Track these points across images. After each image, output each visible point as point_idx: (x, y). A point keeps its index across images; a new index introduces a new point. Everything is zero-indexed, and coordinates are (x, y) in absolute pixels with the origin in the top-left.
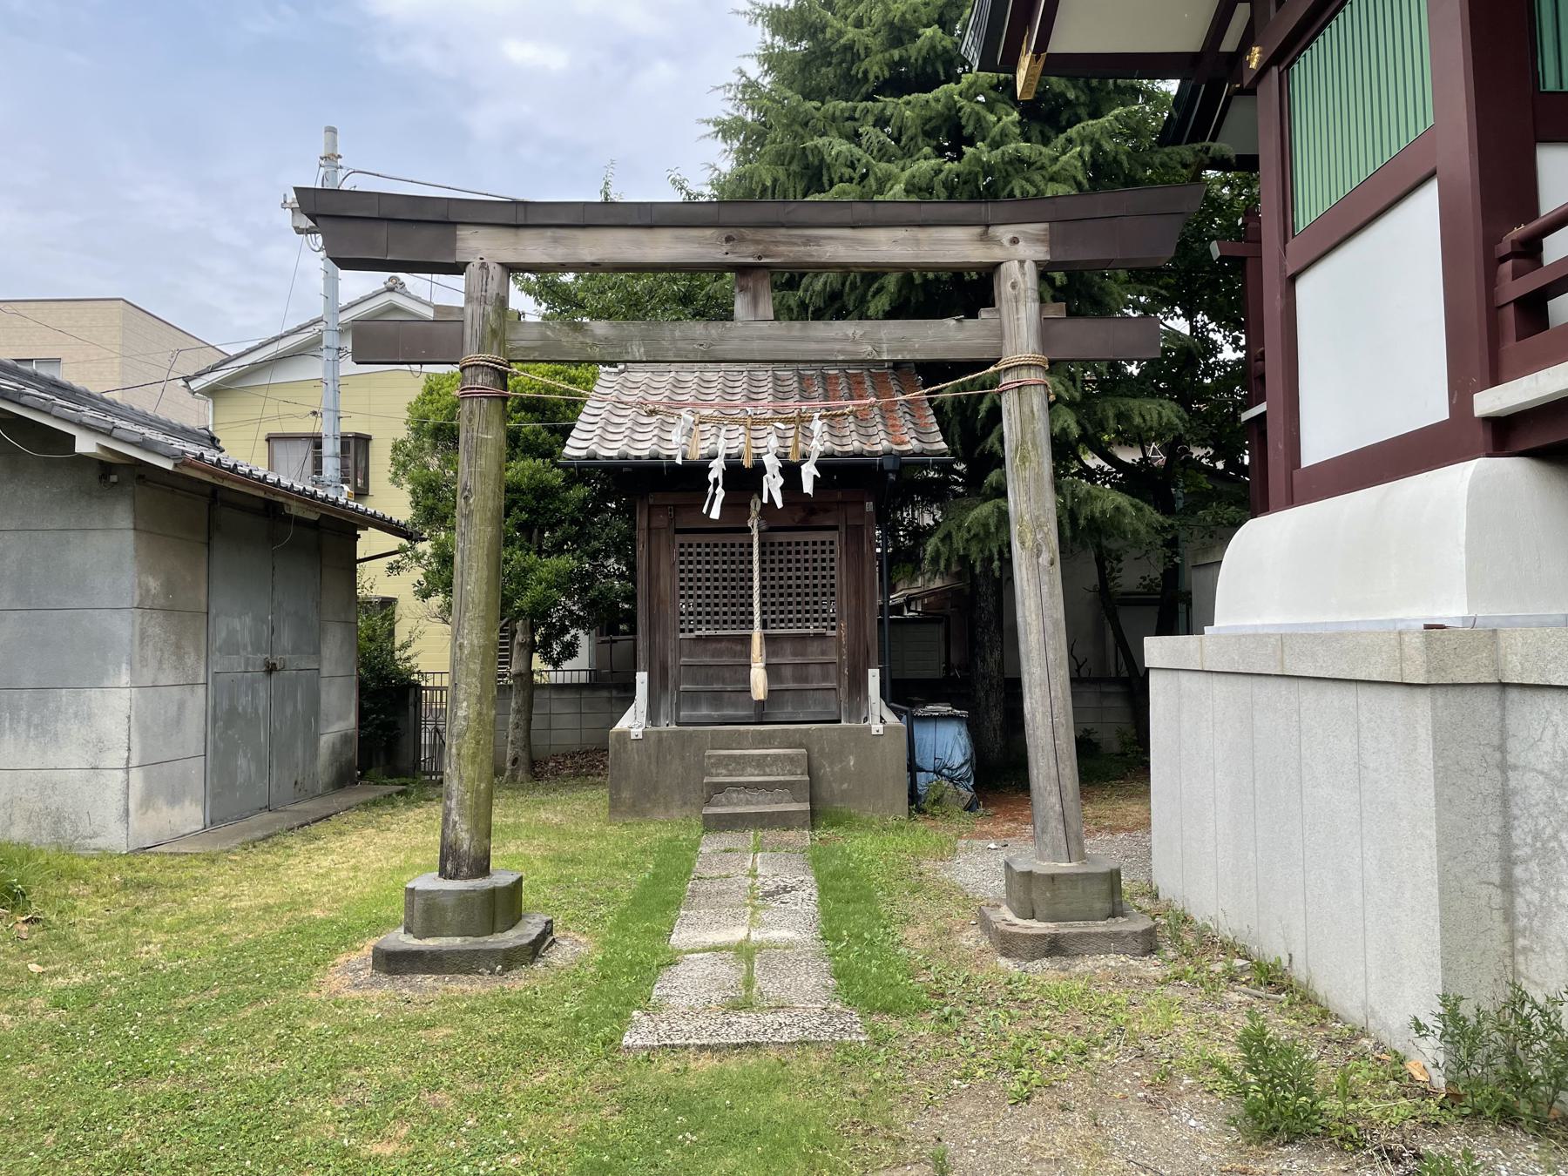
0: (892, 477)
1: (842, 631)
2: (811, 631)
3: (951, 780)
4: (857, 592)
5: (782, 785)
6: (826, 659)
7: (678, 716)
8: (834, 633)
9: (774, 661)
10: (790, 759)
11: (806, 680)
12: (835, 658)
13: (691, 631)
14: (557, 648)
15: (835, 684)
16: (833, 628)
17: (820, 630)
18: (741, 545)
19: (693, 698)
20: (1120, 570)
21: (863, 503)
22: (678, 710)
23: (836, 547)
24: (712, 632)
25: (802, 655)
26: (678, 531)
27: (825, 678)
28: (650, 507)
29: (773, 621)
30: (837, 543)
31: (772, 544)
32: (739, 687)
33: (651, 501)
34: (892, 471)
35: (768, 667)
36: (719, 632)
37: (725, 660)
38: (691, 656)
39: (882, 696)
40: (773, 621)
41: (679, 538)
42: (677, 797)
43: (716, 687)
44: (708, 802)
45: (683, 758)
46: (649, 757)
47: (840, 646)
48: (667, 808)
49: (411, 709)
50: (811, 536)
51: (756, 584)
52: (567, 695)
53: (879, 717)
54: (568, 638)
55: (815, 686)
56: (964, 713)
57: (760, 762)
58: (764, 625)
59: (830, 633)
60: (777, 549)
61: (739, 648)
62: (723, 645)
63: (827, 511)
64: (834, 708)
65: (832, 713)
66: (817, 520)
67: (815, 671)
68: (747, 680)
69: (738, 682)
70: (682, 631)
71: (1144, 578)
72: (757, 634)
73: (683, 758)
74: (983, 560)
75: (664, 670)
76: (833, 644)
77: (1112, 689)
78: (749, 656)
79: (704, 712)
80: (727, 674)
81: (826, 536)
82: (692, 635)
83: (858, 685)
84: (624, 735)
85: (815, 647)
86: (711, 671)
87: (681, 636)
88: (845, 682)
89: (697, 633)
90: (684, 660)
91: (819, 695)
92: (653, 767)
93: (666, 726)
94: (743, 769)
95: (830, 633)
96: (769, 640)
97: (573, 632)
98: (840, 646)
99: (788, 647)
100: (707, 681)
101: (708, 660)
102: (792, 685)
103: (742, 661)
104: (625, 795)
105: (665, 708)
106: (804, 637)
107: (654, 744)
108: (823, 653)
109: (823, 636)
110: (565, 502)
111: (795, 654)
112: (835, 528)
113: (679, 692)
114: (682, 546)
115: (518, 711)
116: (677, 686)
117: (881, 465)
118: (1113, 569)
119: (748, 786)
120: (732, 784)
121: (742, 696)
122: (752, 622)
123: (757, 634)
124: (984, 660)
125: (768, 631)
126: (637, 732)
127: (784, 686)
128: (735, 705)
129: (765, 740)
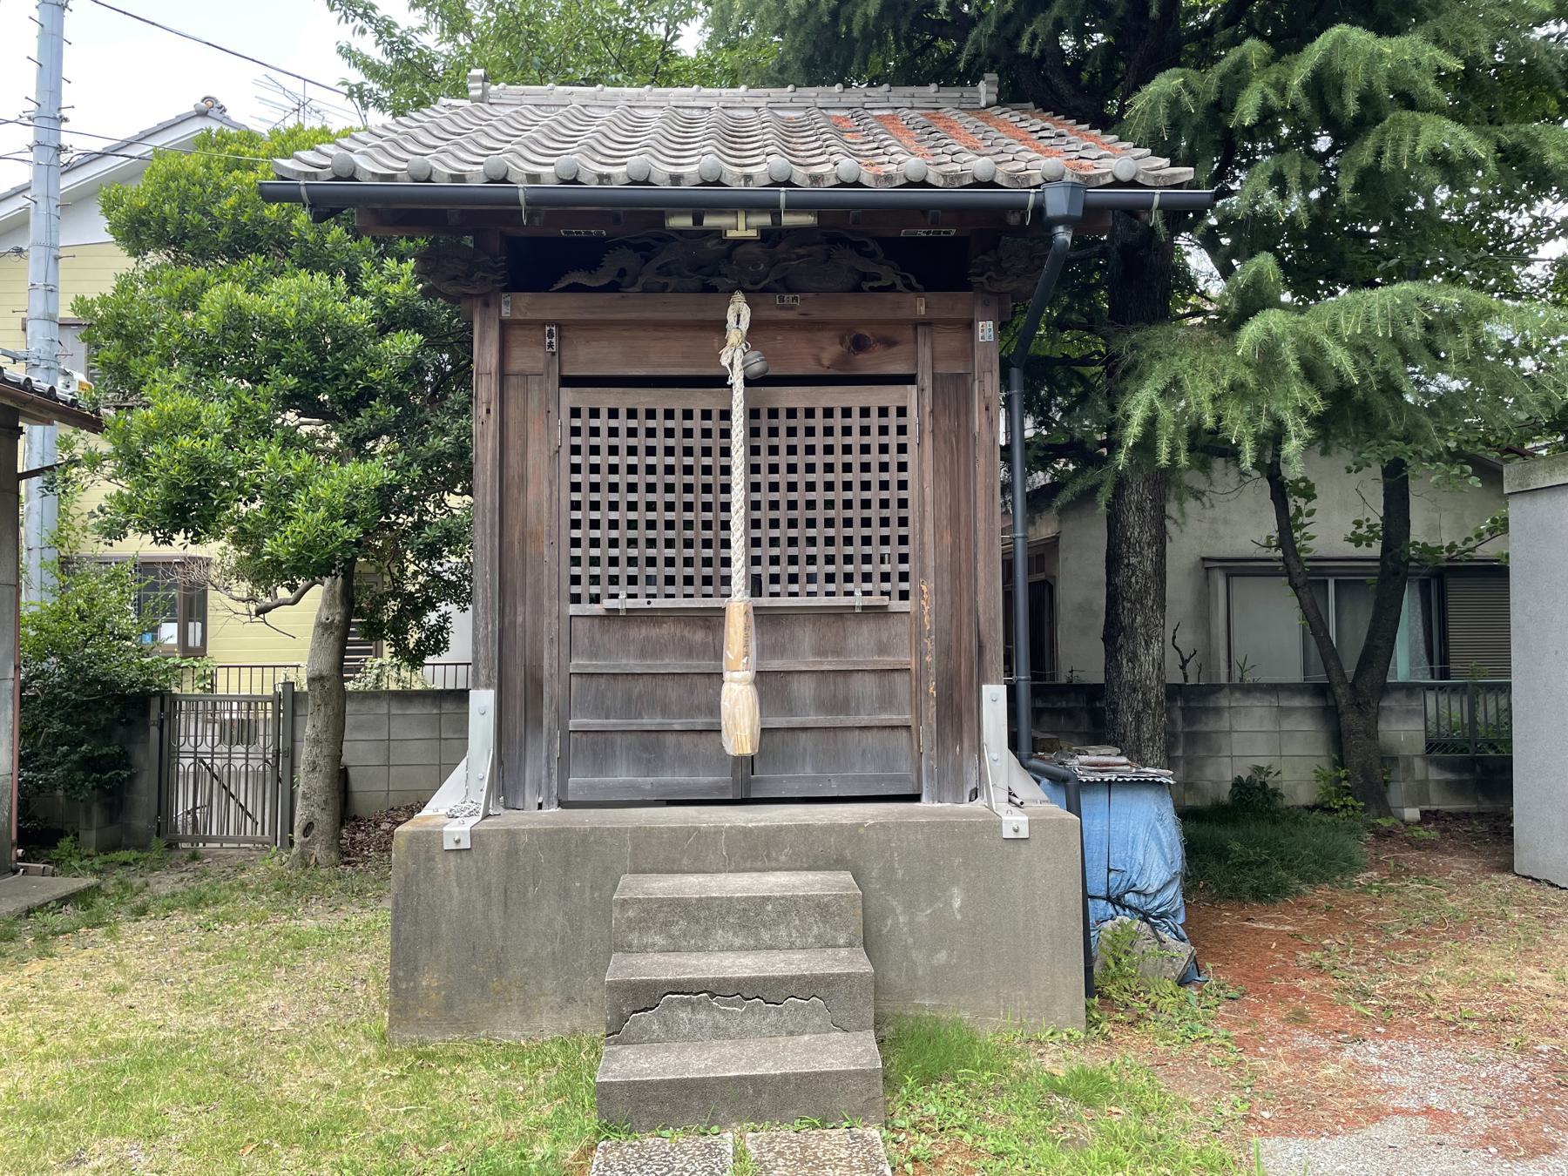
0: (1063, 235)
1: (925, 601)
2: (858, 600)
3: (1145, 917)
4: (954, 519)
5: (808, 986)
6: (888, 661)
7: (563, 786)
8: (905, 606)
9: (775, 665)
10: (821, 908)
11: (843, 706)
12: (907, 659)
13: (595, 599)
14: (413, 637)
15: (907, 717)
16: (904, 595)
17: (876, 600)
18: (706, 415)
19: (599, 746)
20: (1311, 513)
21: (970, 326)
22: (564, 772)
23: (912, 420)
24: (641, 603)
25: (837, 652)
26: (567, 382)
27: (887, 702)
28: (505, 326)
29: (775, 579)
30: (912, 412)
31: (773, 413)
32: (700, 722)
33: (506, 312)
34: (1063, 221)
35: (763, 680)
36: (658, 603)
37: (671, 663)
38: (594, 655)
39: (1013, 744)
40: (775, 579)
41: (569, 397)
42: (549, 985)
43: (649, 722)
44: (616, 1032)
45: (565, 894)
46: (487, 892)
47: (919, 634)
48: (527, 1012)
49: (154, 731)
50: (855, 397)
51: (738, 497)
52: (416, 710)
53: (1011, 800)
54: (432, 618)
55: (864, 720)
56: (1166, 776)
57: (751, 919)
58: (755, 586)
59: (896, 605)
60: (782, 423)
61: (699, 636)
62: (666, 630)
63: (889, 343)
64: (905, 768)
65: (901, 779)
66: (869, 363)
67: (865, 687)
68: (714, 709)
69: (695, 710)
70: (576, 599)
71: (1359, 524)
72: (738, 604)
73: (565, 894)
74: (1259, 439)
75: (535, 684)
76: (901, 628)
77: (1297, 702)
78: (718, 655)
79: (622, 777)
80: (673, 691)
81: (888, 396)
82: (597, 609)
83: (957, 715)
84: (431, 838)
85: (864, 636)
86: (638, 687)
87: (573, 609)
88: (931, 712)
89: (608, 603)
90: (579, 663)
91: (871, 738)
92: (496, 916)
93: (537, 816)
94: (707, 933)
95: (896, 605)
96: (763, 618)
97: (443, 607)
98: (919, 634)
99: (806, 636)
100: (631, 707)
101: (632, 664)
102: (812, 719)
103: (706, 665)
104: (428, 980)
105: (535, 768)
106: (840, 614)
107: (504, 863)
108: (883, 649)
109: (880, 612)
110: (375, 361)
111: (820, 652)
112: (910, 380)
113: (567, 734)
114: (575, 413)
115: (316, 742)
116: (562, 716)
117: (1039, 209)
118: (1299, 509)
119: (718, 990)
120: (677, 988)
121: (705, 741)
122: (726, 580)
123: (738, 604)
124: (1134, 658)
125: (765, 601)
126: (458, 831)
127: (796, 721)
128: (687, 762)
129: (756, 852)
